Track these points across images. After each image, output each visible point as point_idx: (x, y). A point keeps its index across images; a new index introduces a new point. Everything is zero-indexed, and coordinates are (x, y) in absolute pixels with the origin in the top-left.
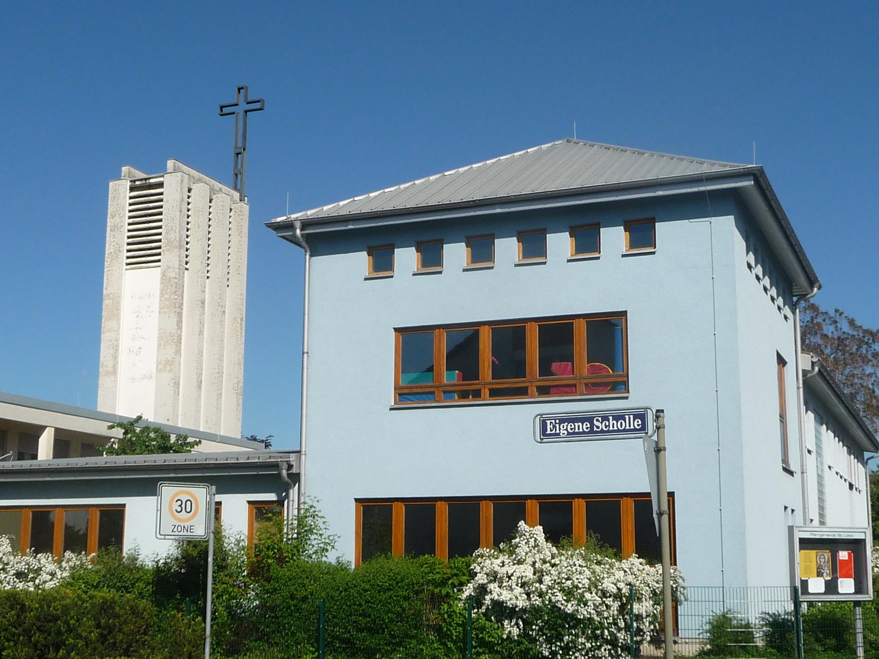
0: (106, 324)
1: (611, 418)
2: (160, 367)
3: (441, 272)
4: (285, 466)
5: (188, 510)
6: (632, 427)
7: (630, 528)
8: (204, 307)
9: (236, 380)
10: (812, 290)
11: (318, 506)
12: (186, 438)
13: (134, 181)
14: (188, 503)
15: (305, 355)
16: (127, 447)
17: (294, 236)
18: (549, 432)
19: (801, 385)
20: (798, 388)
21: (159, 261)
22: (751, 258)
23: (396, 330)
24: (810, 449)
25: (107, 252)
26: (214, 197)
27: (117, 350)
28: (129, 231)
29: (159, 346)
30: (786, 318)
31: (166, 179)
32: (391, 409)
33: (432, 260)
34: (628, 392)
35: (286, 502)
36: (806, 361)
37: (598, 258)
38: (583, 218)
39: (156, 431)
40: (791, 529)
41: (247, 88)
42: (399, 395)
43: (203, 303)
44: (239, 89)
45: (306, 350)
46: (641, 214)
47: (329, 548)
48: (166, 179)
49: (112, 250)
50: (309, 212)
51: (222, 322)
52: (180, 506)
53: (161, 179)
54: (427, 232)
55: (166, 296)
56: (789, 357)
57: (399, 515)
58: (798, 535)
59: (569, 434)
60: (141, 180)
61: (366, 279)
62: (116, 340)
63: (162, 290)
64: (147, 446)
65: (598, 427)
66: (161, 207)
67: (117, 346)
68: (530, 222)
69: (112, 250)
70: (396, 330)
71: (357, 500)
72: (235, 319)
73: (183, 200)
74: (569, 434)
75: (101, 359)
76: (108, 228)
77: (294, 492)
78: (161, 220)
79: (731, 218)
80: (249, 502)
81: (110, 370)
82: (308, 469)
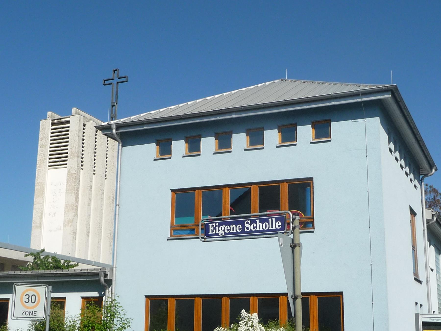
0: (37, 199)
1: (258, 221)
2: (66, 223)
3: (199, 155)
4: (103, 275)
5: (33, 301)
6: (274, 228)
7: (315, 315)
8: (91, 190)
9: (110, 232)
10: (432, 171)
11: (118, 300)
12: (69, 262)
13: (54, 120)
14: (34, 297)
15: (117, 206)
16: (36, 266)
17: (112, 134)
18: (210, 233)
19: (426, 229)
20: (424, 230)
21: (66, 164)
22: (392, 146)
23: (172, 191)
24: (433, 268)
25: (38, 159)
26: (87, 123)
27: (42, 214)
28: (51, 148)
29: (65, 211)
30: (415, 187)
31: (71, 119)
32: (168, 240)
33: (194, 148)
34: (314, 228)
35: (104, 298)
36: (428, 214)
37: (295, 145)
38: (287, 119)
39: (53, 258)
40: (417, 316)
41: (127, 77)
42: (174, 230)
43: (91, 188)
44: (114, 71)
45: (118, 204)
46: (322, 117)
47: (126, 326)
48: (71, 119)
49: (41, 158)
50: (122, 120)
51: (102, 199)
52: (28, 298)
53: (69, 119)
54: (192, 131)
55: (70, 184)
56: (418, 209)
57: (172, 305)
58: (422, 320)
59: (226, 234)
60: (58, 119)
61: (155, 160)
62: (42, 208)
63: (67, 181)
64: (46, 267)
65: (248, 228)
66: (68, 134)
67: (42, 212)
68: (253, 123)
69: (41, 158)
70: (172, 191)
71: (146, 296)
72: (110, 197)
73: (80, 130)
74: (226, 234)
75: (33, 220)
76: (39, 147)
77: (108, 292)
78: (68, 142)
79: (378, 118)
80: (82, 298)
81: (38, 225)
82: (117, 278)
